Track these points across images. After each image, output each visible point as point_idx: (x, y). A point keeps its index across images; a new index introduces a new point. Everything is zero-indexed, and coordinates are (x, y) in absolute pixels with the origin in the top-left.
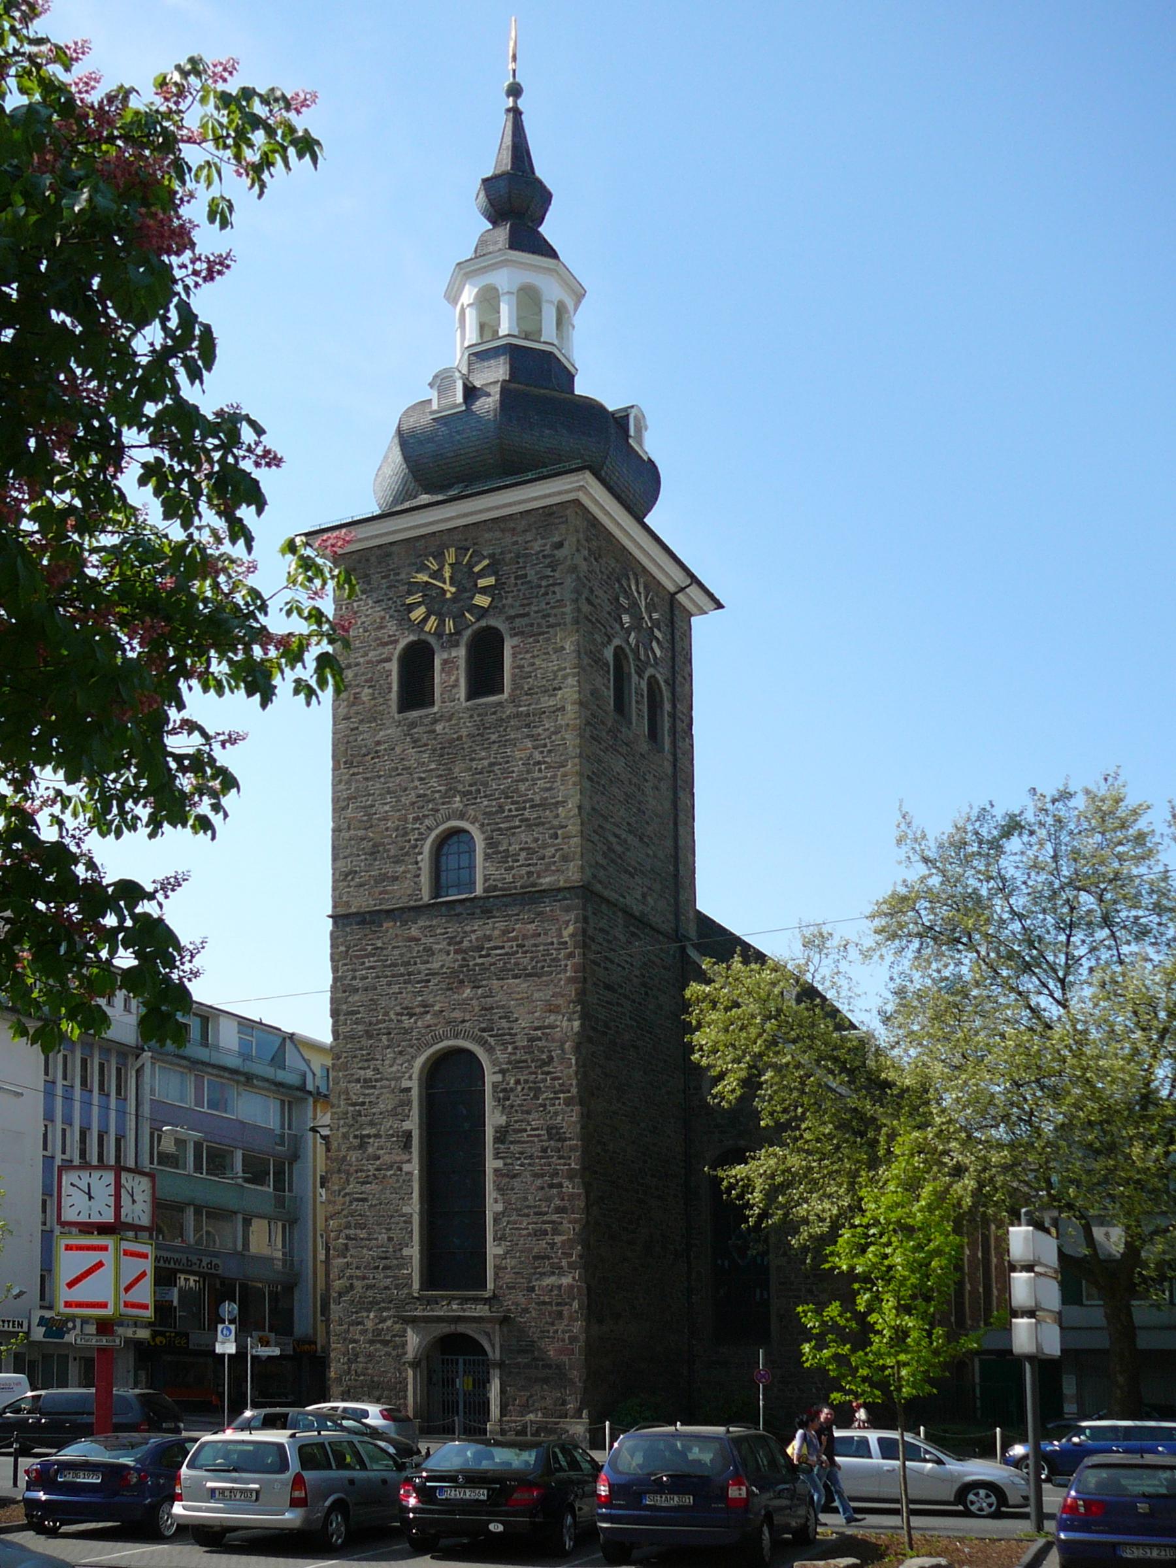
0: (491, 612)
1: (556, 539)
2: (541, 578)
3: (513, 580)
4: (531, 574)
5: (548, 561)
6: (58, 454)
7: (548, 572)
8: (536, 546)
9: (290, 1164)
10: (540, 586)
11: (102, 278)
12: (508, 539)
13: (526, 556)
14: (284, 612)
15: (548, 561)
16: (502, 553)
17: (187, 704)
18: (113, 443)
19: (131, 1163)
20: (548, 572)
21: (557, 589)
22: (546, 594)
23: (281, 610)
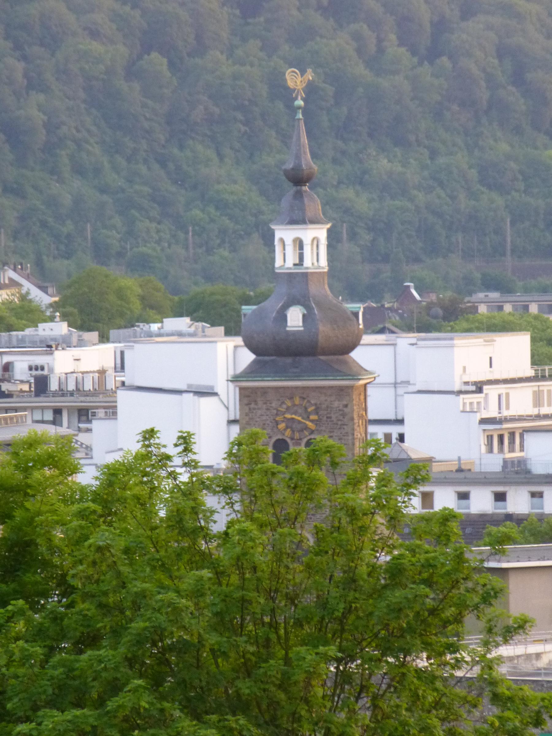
0: (316, 432)
1: (345, 403)
2: (339, 420)
3: (325, 418)
4: (334, 417)
5: (341, 412)
6: (284, 234)
7: (341, 418)
8: (336, 404)
9: (522, 436)
10: (337, 424)
11: (60, 300)
12: (323, 398)
13: (331, 407)
14: (180, 434)
15: (341, 412)
16: (320, 404)
17: (211, 384)
18: (303, 246)
19: (468, 409)
20: (341, 418)
21: (345, 427)
22: (340, 428)
23: (181, 432)
